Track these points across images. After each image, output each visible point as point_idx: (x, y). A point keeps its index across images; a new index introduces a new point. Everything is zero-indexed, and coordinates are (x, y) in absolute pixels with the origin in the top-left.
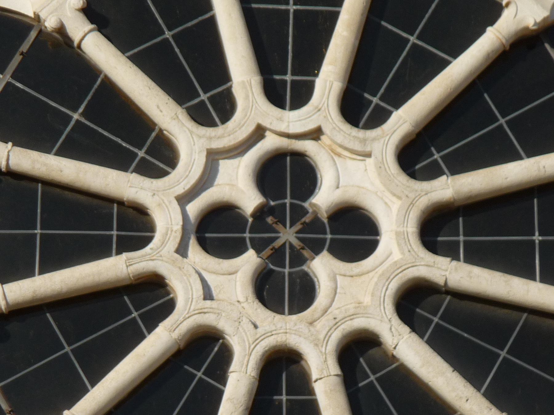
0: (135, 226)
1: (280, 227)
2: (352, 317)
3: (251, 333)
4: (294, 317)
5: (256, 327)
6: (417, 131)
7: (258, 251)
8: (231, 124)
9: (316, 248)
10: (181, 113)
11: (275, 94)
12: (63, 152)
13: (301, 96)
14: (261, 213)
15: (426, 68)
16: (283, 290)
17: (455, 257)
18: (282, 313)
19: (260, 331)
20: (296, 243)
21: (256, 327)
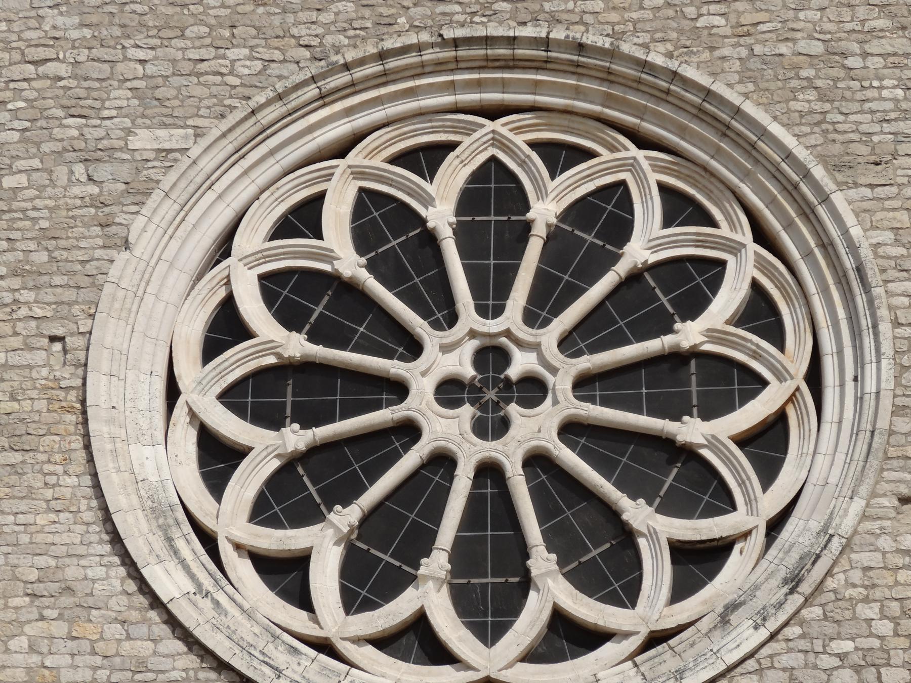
0: (584, 385)
1: (496, 390)
2: (529, 440)
3: (470, 453)
4: (493, 443)
5: (539, 431)
6: (367, 291)
7: (472, 405)
8: (454, 329)
9: (508, 401)
10: (425, 324)
11: (482, 311)
12: (353, 350)
13: (498, 311)
14: (507, 380)
15: (573, 293)
16: (492, 426)
17: (594, 403)
18: (488, 440)
19: (541, 435)
20: (495, 399)
21: (539, 431)
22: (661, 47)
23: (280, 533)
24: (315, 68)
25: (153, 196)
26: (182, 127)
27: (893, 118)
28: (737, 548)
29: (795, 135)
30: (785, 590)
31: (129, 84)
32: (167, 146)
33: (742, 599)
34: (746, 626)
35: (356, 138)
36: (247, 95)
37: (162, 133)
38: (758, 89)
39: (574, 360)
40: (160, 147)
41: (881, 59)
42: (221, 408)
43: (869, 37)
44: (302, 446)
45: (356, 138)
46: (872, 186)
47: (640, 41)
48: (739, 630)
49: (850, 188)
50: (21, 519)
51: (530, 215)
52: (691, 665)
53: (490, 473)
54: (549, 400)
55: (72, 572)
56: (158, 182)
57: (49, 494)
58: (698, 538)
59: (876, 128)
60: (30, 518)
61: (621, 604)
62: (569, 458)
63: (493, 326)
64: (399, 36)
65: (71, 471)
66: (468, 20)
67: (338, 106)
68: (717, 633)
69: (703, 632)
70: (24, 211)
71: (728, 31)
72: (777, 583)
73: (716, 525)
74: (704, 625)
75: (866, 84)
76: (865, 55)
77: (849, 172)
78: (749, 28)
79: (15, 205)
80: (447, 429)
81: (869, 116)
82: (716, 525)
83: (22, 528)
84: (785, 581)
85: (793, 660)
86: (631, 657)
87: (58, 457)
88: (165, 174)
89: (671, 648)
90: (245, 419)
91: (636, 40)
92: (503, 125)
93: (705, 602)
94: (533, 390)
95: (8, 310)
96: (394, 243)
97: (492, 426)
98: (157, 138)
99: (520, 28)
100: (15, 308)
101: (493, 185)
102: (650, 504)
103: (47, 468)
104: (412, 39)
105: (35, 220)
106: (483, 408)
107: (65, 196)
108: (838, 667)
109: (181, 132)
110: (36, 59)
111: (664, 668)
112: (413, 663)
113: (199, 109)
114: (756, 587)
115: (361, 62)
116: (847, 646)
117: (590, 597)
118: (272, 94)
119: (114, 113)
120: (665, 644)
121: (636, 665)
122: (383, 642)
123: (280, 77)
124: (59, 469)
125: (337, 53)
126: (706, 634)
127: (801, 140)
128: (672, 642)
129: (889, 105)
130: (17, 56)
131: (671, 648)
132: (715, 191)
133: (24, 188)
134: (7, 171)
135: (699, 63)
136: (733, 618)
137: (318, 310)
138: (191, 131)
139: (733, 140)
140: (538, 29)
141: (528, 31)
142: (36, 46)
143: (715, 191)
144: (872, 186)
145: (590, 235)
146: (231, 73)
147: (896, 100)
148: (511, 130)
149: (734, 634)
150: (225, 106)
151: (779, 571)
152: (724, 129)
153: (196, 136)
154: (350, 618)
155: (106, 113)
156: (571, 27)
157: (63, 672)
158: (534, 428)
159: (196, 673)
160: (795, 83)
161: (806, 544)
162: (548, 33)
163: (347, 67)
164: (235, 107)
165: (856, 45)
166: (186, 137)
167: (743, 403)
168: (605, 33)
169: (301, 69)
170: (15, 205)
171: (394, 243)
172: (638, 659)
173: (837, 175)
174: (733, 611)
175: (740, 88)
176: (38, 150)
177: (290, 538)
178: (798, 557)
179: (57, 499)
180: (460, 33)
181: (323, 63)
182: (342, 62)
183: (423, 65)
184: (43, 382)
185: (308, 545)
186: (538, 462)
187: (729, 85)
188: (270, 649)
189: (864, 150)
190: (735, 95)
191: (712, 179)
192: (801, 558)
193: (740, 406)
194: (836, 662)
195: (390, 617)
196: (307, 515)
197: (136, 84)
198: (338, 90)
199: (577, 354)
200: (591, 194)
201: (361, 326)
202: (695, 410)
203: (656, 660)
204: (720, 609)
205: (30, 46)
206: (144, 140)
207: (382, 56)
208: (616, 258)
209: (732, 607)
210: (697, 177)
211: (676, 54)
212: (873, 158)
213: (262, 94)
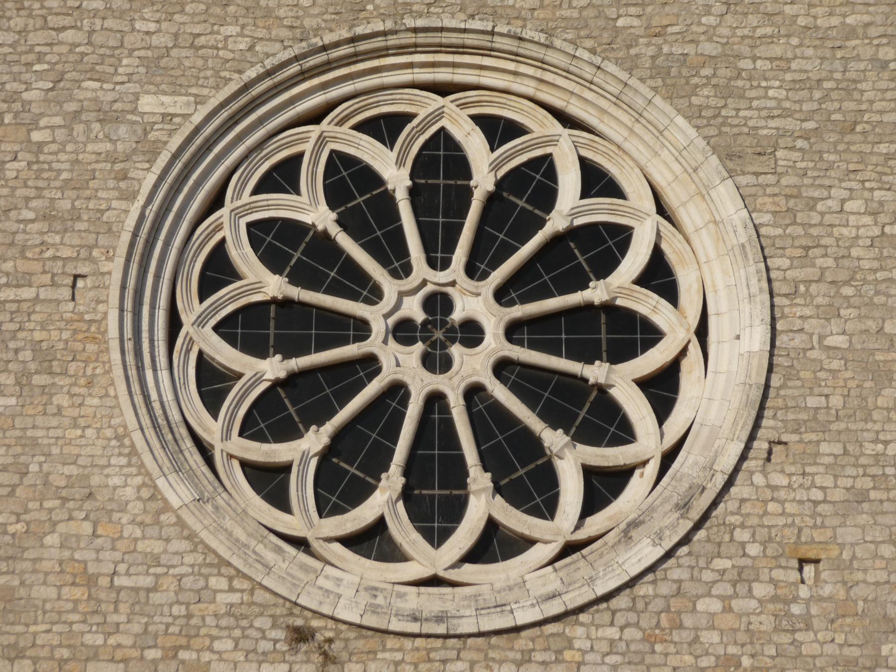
2: (471, 376)
3: (421, 385)
7: (424, 343)
8: (410, 278)
9: (453, 341)
10: (385, 272)
11: (432, 263)
13: (445, 264)
22: (589, 43)
23: (266, 447)
24: (299, 48)
25: (161, 155)
26: (184, 95)
27: (776, 114)
28: (637, 472)
29: (694, 127)
30: (677, 515)
31: (136, 53)
32: (171, 110)
33: (641, 518)
34: (645, 543)
35: (330, 107)
36: (240, 68)
37: (166, 99)
38: (665, 85)
39: (508, 310)
40: (166, 111)
41: (768, 62)
42: (216, 338)
43: (758, 42)
44: (282, 375)
45: (330, 107)
46: (757, 174)
47: (569, 36)
48: (639, 546)
49: (738, 175)
50: (52, 433)
51: (472, 183)
52: (601, 574)
53: (435, 400)
54: (449, 290)
55: (95, 480)
56: (166, 143)
57: (75, 412)
58: (606, 464)
59: (762, 123)
60: (59, 433)
61: (543, 517)
62: (501, 393)
63: (442, 277)
64: (369, 23)
65: (94, 393)
66: (426, 11)
67: (316, 81)
68: (622, 547)
69: (610, 544)
70: (49, 163)
71: (641, 32)
72: (669, 507)
73: (621, 453)
74: (611, 538)
75: (755, 84)
76: (754, 59)
77: (739, 161)
78: (660, 29)
79: (42, 158)
80: (402, 363)
81: (756, 112)
82: (621, 453)
83: (52, 441)
84: (677, 507)
85: (684, 574)
86: (551, 562)
87: (82, 381)
88: (170, 135)
89: (584, 557)
90: (236, 348)
91: (566, 36)
92: (452, 102)
93: (610, 518)
94: (471, 334)
95: (37, 250)
96: (360, 200)
97: (438, 362)
98: (163, 104)
99: (470, 21)
100: (44, 248)
101: (441, 153)
102: (567, 433)
103: (76, 390)
104: (379, 26)
105: (59, 172)
106: (433, 345)
107: (84, 151)
108: (718, 581)
109: (185, 99)
110: (56, 26)
111: (579, 575)
112: (374, 560)
113: (198, 78)
114: (651, 509)
115: (337, 45)
116: (728, 564)
117: (517, 508)
118: (262, 70)
119: (125, 78)
120: (578, 553)
121: (555, 570)
122: (352, 542)
123: (268, 55)
124: (83, 391)
125: (315, 36)
126: (613, 547)
127: (700, 131)
128: (585, 551)
129: (772, 104)
130: (39, 22)
131: (584, 557)
132: (627, 167)
133: (49, 142)
134: (34, 127)
135: (617, 59)
136: (633, 533)
137: (297, 255)
138: (192, 99)
139: (644, 126)
140: (485, 23)
141: (476, 25)
142: (57, 14)
143: (627, 167)
144: (757, 174)
145: (521, 199)
146: (225, 48)
147: (779, 101)
148: (458, 106)
149: (635, 549)
150: (220, 77)
151: (672, 497)
152: (637, 116)
153: (196, 103)
154: (323, 520)
155: (119, 79)
156: (512, 21)
157: (90, 565)
158: (472, 365)
159: (200, 569)
160: (696, 80)
161: (694, 475)
162: (494, 27)
163: (324, 48)
164: (230, 79)
165: (747, 48)
166: (188, 104)
167: (644, 350)
168: (540, 28)
169: (285, 48)
170: (42, 158)
171: (360, 200)
172: (558, 565)
173: (728, 162)
174: (634, 528)
175: (650, 82)
176: (61, 108)
177: (274, 451)
178: (687, 486)
179: (83, 416)
180: (420, 23)
181: (304, 44)
182: (320, 44)
183: (387, 48)
184: (69, 315)
185: (290, 459)
186: (474, 393)
187: (642, 80)
188: (260, 548)
189: (748, 141)
190: (648, 90)
191: (625, 157)
192: (690, 488)
193: (642, 353)
194: (716, 576)
195: (356, 521)
196: (287, 432)
197: (142, 53)
198: (316, 67)
199: (511, 304)
200: (524, 164)
201: (332, 271)
202: (604, 355)
203: (572, 567)
204: (623, 526)
205: (50, 14)
206: (148, 103)
207: (353, 40)
208: (541, 223)
209: (634, 524)
210: (611, 154)
211: (599, 50)
212: (759, 150)
213: (253, 69)
